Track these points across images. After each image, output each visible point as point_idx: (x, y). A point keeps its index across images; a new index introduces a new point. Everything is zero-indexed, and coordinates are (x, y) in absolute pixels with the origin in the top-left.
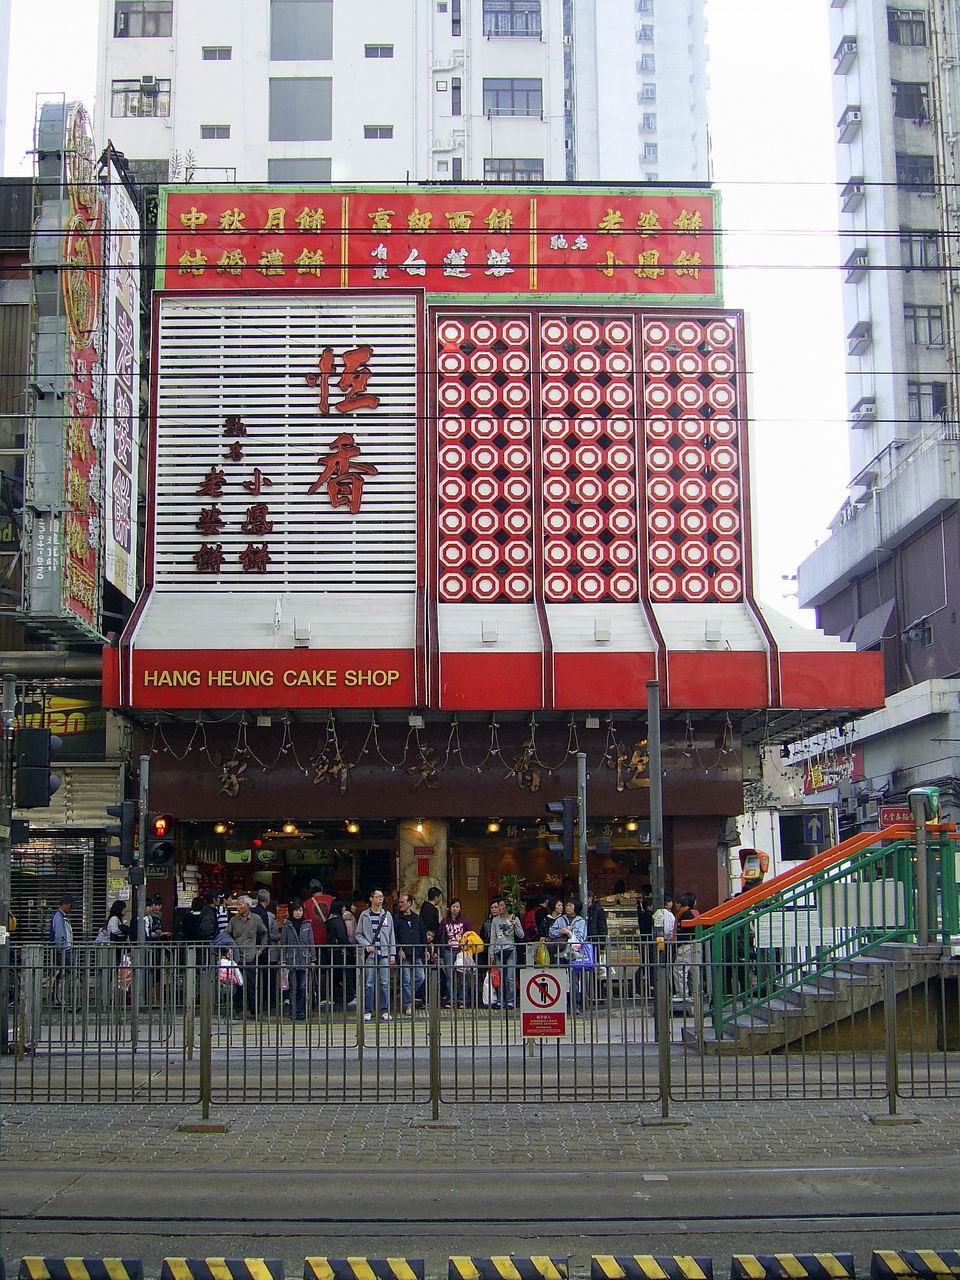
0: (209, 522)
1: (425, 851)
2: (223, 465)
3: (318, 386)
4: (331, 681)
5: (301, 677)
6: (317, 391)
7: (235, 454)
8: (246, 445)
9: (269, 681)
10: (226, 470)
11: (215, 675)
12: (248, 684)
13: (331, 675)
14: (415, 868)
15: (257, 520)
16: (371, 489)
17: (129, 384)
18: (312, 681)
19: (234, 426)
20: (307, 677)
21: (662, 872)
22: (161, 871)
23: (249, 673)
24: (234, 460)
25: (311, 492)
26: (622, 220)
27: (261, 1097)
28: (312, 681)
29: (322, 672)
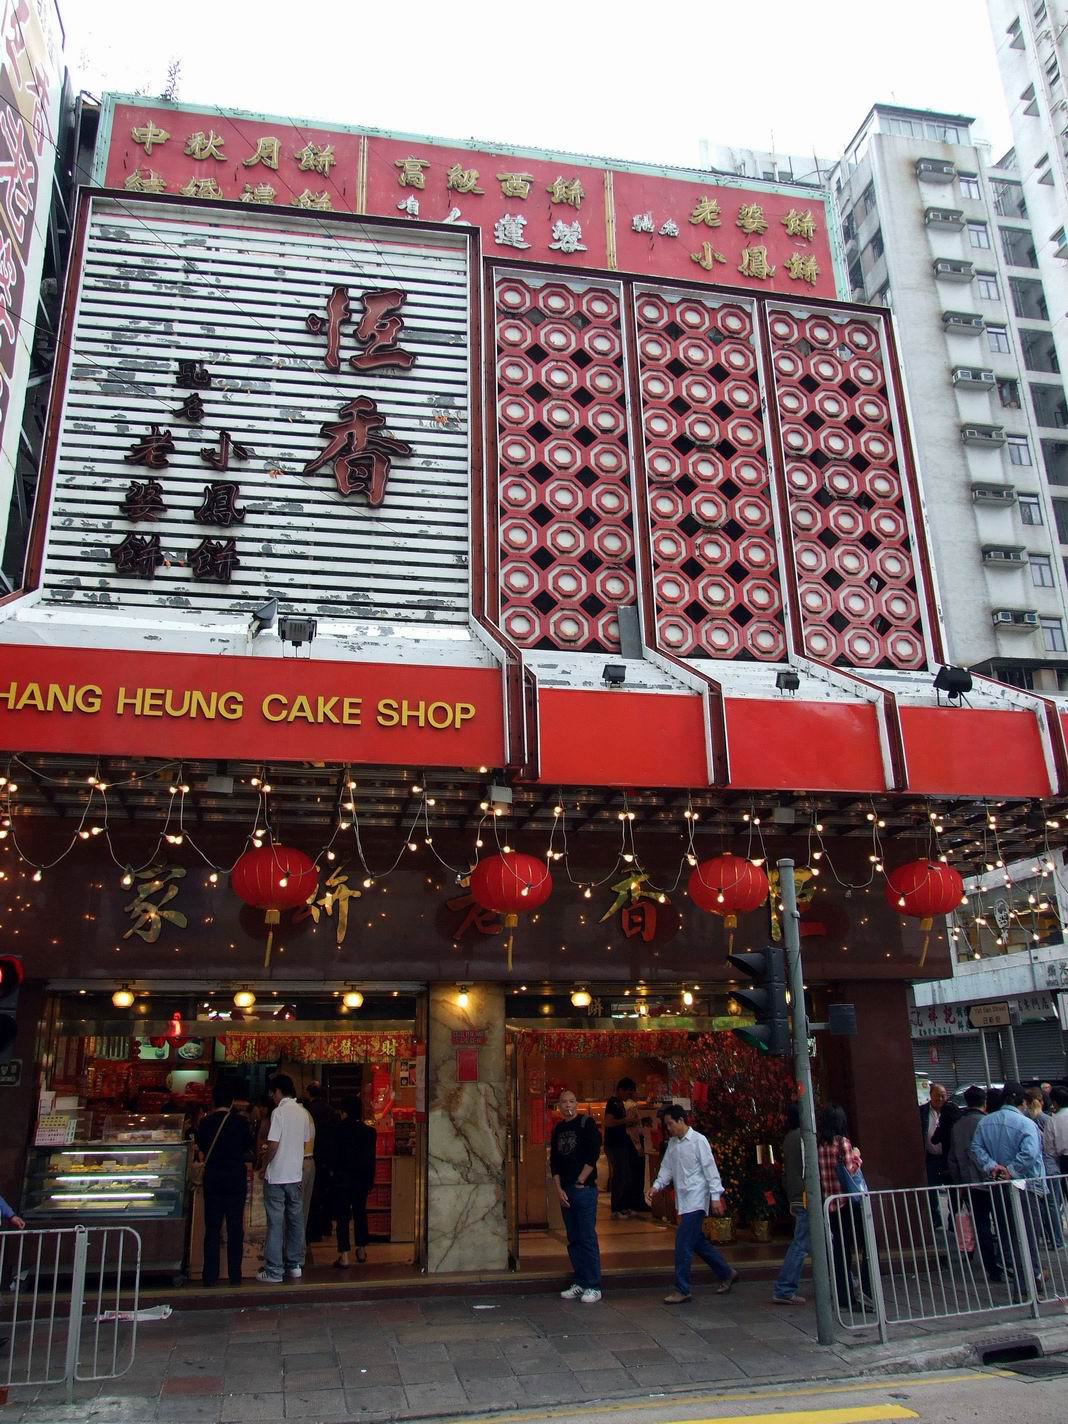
0: (143, 502)
1: (470, 1037)
2: (171, 425)
3: (325, 334)
4: (352, 716)
5: (296, 706)
6: (322, 340)
7: (192, 412)
8: (209, 402)
9: (234, 711)
10: (175, 432)
11: (131, 694)
12: (193, 714)
13: (352, 705)
14: (452, 1066)
15: (220, 506)
16: (403, 482)
17: (21, 241)
18: (315, 715)
19: (191, 375)
20: (307, 707)
21: (1029, 1079)
22: (9, 1074)
23: (198, 695)
24: (190, 420)
25: (307, 473)
26: (718, 209)
27: (104, 589)
28: (315, 715)
29: (334, 700)
